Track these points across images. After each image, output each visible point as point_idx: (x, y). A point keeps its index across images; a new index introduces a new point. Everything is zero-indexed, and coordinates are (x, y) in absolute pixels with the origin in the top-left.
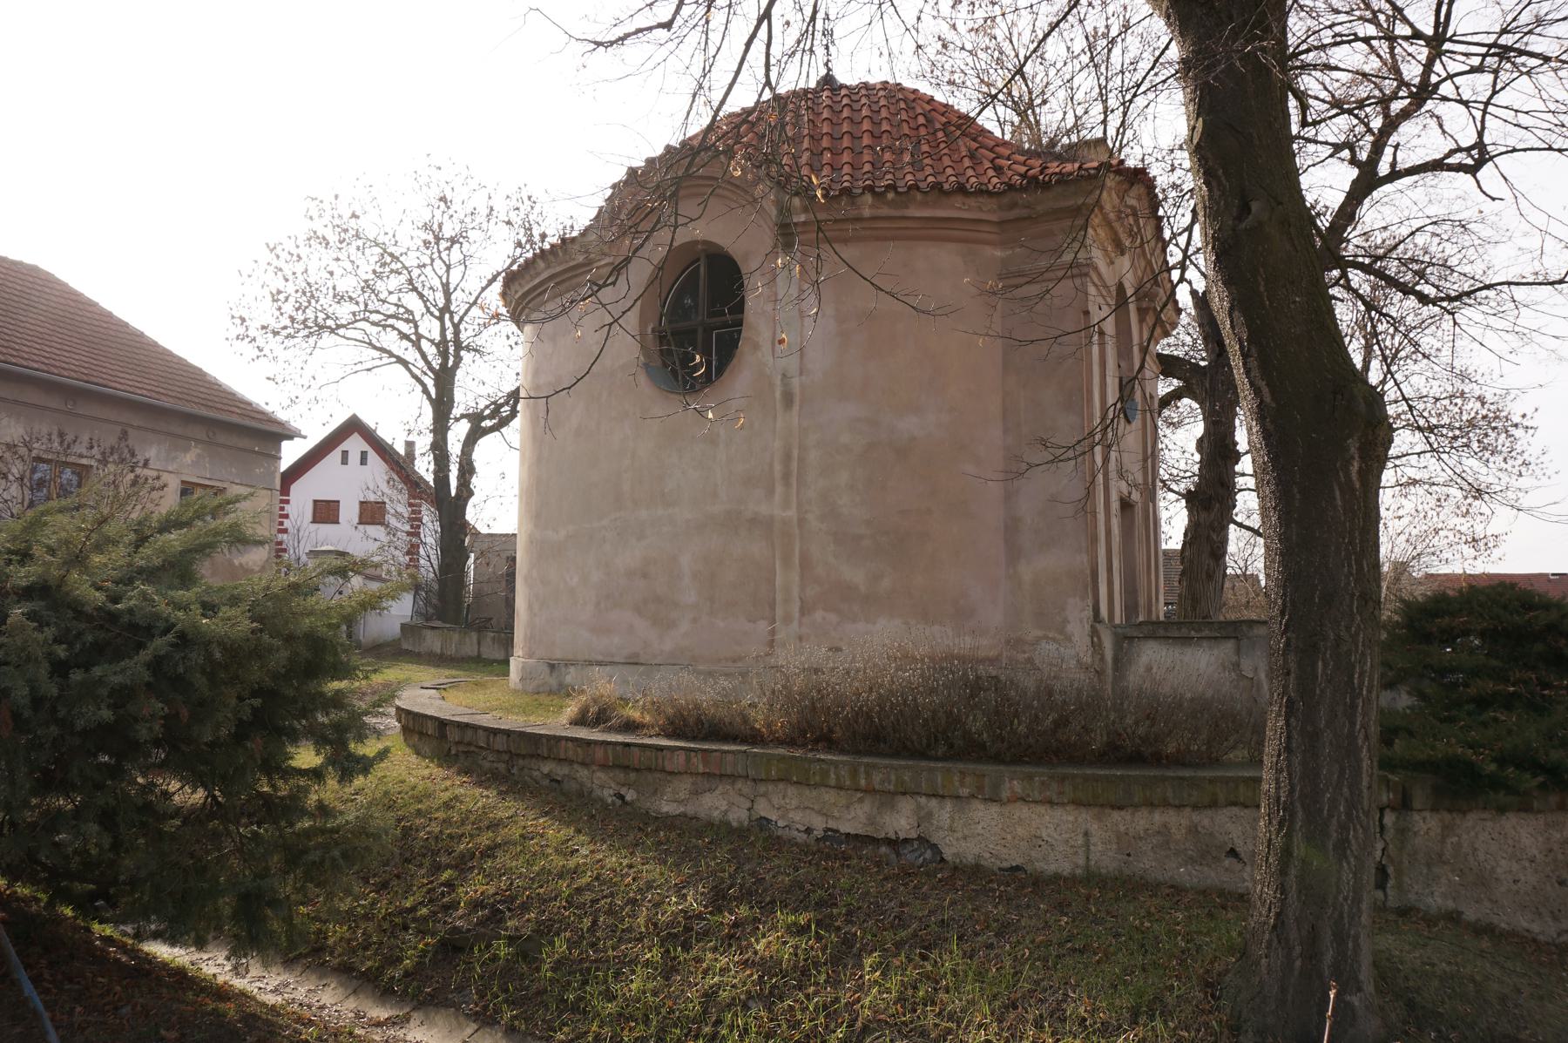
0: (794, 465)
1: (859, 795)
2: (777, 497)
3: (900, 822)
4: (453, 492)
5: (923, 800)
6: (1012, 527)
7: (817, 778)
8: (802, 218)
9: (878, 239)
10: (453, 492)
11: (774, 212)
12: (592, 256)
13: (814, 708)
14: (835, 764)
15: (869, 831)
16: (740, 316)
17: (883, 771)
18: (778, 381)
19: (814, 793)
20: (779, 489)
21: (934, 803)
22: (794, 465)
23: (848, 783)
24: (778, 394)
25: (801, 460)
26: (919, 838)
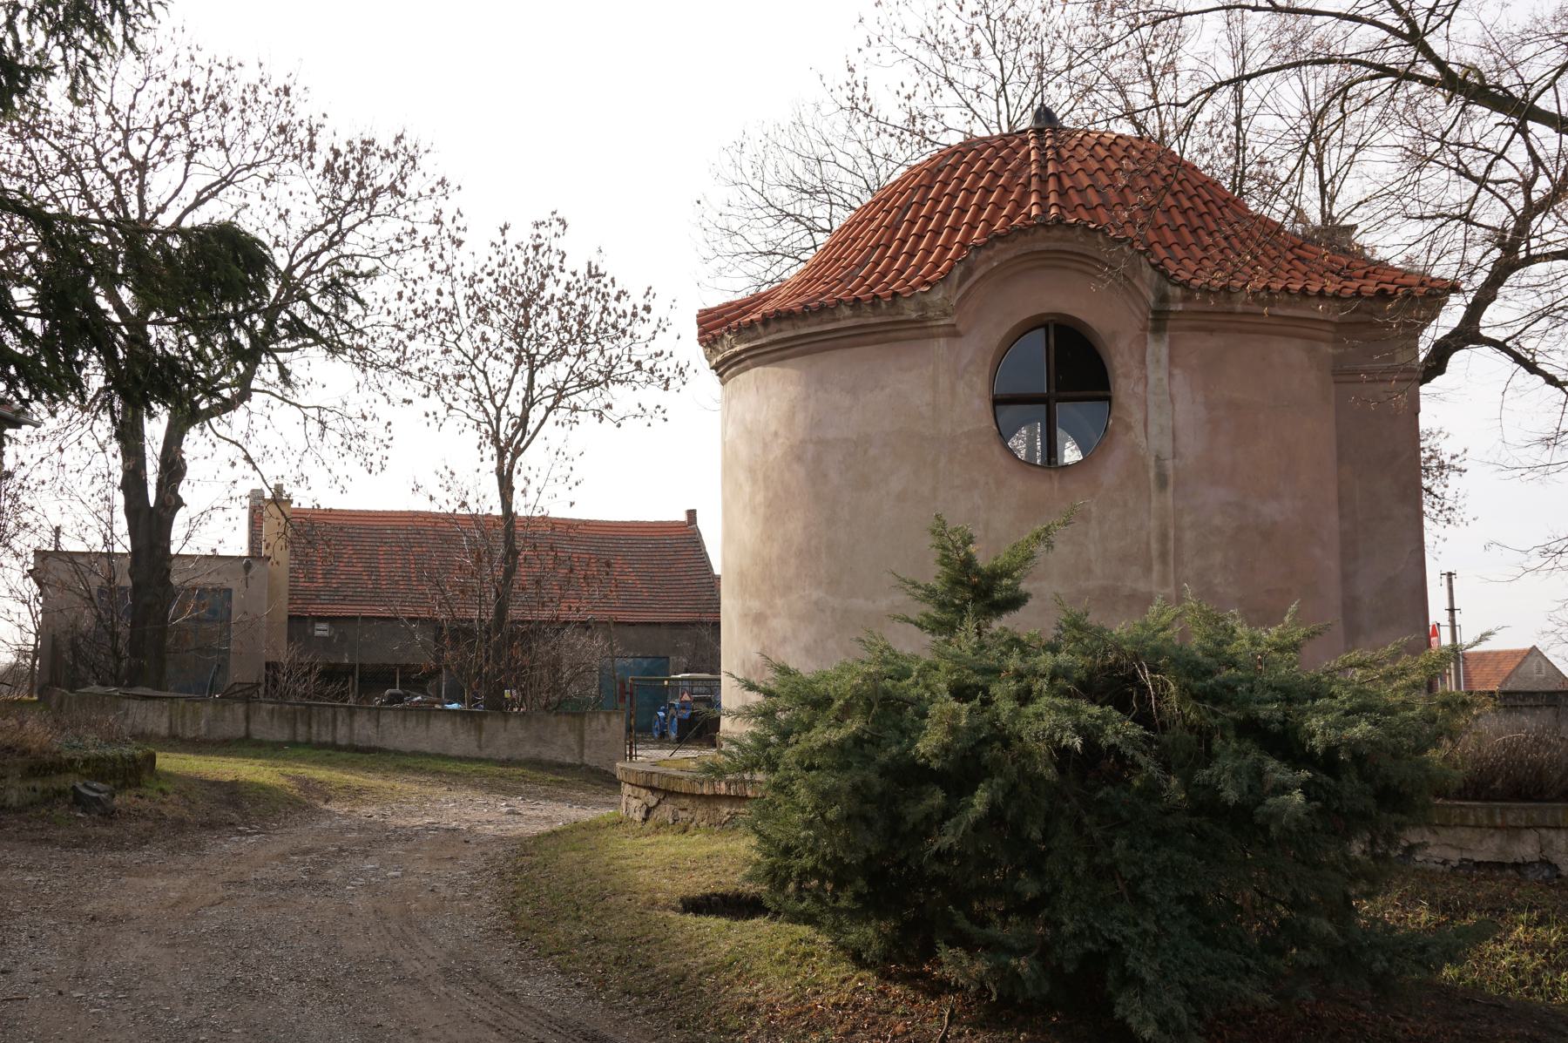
0: (1171, 545)
1: (1492, 831)
2: (1155, 575)
3: (1526, 849)
4: (152, 503)
5: (1544, 831)
6: (1350, 606)
7: (1457, 820)
8: (1180, 307)
9: (1240, 331)
10: (152, 503)
11: (1152, 298)
12: (930, 314)
13: (1521, 762)
14: (1474, 808)
15: (1501, 858)
16: (1107, 393)
17: (1516, 813)
18: (1152, 462)
19: (1451, 832)
20: (1156, 567)
21: (1552, 833)
22: (1171, 545)
23: (1486, 822)
24: (1152, 475)
25: (1178, 540)
26: (1541, 861)
